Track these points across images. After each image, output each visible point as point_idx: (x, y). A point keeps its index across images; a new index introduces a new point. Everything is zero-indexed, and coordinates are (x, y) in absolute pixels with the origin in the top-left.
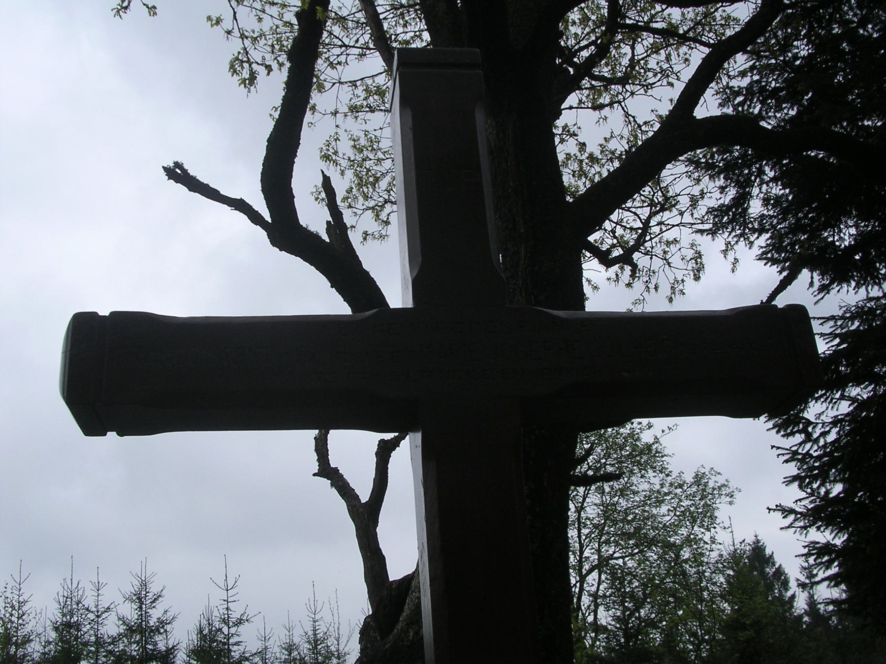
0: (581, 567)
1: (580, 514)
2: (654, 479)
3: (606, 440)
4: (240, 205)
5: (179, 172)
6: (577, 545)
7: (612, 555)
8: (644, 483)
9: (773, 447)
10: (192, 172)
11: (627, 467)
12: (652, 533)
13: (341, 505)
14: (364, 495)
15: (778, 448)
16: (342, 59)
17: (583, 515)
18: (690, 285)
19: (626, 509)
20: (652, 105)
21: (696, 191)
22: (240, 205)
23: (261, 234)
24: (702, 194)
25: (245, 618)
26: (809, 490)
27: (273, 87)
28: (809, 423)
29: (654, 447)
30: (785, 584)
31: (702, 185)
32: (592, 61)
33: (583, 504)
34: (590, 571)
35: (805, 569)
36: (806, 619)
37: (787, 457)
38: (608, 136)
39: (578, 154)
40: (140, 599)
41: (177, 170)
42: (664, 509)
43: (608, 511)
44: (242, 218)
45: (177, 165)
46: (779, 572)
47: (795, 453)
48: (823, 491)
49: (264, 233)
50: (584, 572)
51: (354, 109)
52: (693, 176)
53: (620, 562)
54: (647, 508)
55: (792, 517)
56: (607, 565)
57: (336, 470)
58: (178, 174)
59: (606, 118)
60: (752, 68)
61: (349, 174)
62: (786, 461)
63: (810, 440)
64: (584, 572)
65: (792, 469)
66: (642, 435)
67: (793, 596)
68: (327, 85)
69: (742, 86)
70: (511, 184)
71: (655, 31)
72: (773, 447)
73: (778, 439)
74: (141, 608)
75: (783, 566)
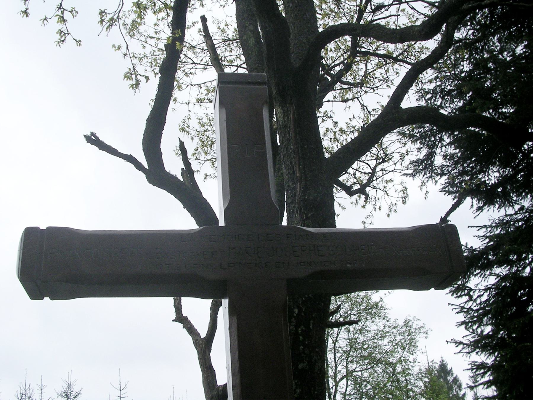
3: (351, 300)
4: (130, 159)
5: (94, 138)
6: (333, 363)
8: (374, 326)
9: (449, 304)
12: (379, 356)
13: (189, 339)
15: (452, 305)
17: (337, 345)
19: (363, 342)
20: (377, 100)
21: (403, 150)
22: (130, 159)
23: (142, 176)
26: (471, 330)
28: (471, 289)
29: (380, 304)
30: (460, 387)
32: (341, 74)
34: (342, 379)
39: (333, 128)
40: (67, 395)
41: (92, 137)
42: (386, 341)
43: (352, 343)
44: (131, 166)
45: (93, 134)
46: (456, 380)
47: (463, 308)
48: (479, 330)
50: (338, 380)
54: (376, 341)
55: (461, 346)
57: (186, 318)
58: (93, 140)
60: (436, 78)
61: (197, 139)
62: (458, 313)
63: (471, 300)
64: (338, 380)
65: (461, 317)
66: (372, 297)
67: (464, 395)
68: (184, 86)
70: (292, 147)
71: (379, 56)
72: (449, 304)
75: (458, 376)
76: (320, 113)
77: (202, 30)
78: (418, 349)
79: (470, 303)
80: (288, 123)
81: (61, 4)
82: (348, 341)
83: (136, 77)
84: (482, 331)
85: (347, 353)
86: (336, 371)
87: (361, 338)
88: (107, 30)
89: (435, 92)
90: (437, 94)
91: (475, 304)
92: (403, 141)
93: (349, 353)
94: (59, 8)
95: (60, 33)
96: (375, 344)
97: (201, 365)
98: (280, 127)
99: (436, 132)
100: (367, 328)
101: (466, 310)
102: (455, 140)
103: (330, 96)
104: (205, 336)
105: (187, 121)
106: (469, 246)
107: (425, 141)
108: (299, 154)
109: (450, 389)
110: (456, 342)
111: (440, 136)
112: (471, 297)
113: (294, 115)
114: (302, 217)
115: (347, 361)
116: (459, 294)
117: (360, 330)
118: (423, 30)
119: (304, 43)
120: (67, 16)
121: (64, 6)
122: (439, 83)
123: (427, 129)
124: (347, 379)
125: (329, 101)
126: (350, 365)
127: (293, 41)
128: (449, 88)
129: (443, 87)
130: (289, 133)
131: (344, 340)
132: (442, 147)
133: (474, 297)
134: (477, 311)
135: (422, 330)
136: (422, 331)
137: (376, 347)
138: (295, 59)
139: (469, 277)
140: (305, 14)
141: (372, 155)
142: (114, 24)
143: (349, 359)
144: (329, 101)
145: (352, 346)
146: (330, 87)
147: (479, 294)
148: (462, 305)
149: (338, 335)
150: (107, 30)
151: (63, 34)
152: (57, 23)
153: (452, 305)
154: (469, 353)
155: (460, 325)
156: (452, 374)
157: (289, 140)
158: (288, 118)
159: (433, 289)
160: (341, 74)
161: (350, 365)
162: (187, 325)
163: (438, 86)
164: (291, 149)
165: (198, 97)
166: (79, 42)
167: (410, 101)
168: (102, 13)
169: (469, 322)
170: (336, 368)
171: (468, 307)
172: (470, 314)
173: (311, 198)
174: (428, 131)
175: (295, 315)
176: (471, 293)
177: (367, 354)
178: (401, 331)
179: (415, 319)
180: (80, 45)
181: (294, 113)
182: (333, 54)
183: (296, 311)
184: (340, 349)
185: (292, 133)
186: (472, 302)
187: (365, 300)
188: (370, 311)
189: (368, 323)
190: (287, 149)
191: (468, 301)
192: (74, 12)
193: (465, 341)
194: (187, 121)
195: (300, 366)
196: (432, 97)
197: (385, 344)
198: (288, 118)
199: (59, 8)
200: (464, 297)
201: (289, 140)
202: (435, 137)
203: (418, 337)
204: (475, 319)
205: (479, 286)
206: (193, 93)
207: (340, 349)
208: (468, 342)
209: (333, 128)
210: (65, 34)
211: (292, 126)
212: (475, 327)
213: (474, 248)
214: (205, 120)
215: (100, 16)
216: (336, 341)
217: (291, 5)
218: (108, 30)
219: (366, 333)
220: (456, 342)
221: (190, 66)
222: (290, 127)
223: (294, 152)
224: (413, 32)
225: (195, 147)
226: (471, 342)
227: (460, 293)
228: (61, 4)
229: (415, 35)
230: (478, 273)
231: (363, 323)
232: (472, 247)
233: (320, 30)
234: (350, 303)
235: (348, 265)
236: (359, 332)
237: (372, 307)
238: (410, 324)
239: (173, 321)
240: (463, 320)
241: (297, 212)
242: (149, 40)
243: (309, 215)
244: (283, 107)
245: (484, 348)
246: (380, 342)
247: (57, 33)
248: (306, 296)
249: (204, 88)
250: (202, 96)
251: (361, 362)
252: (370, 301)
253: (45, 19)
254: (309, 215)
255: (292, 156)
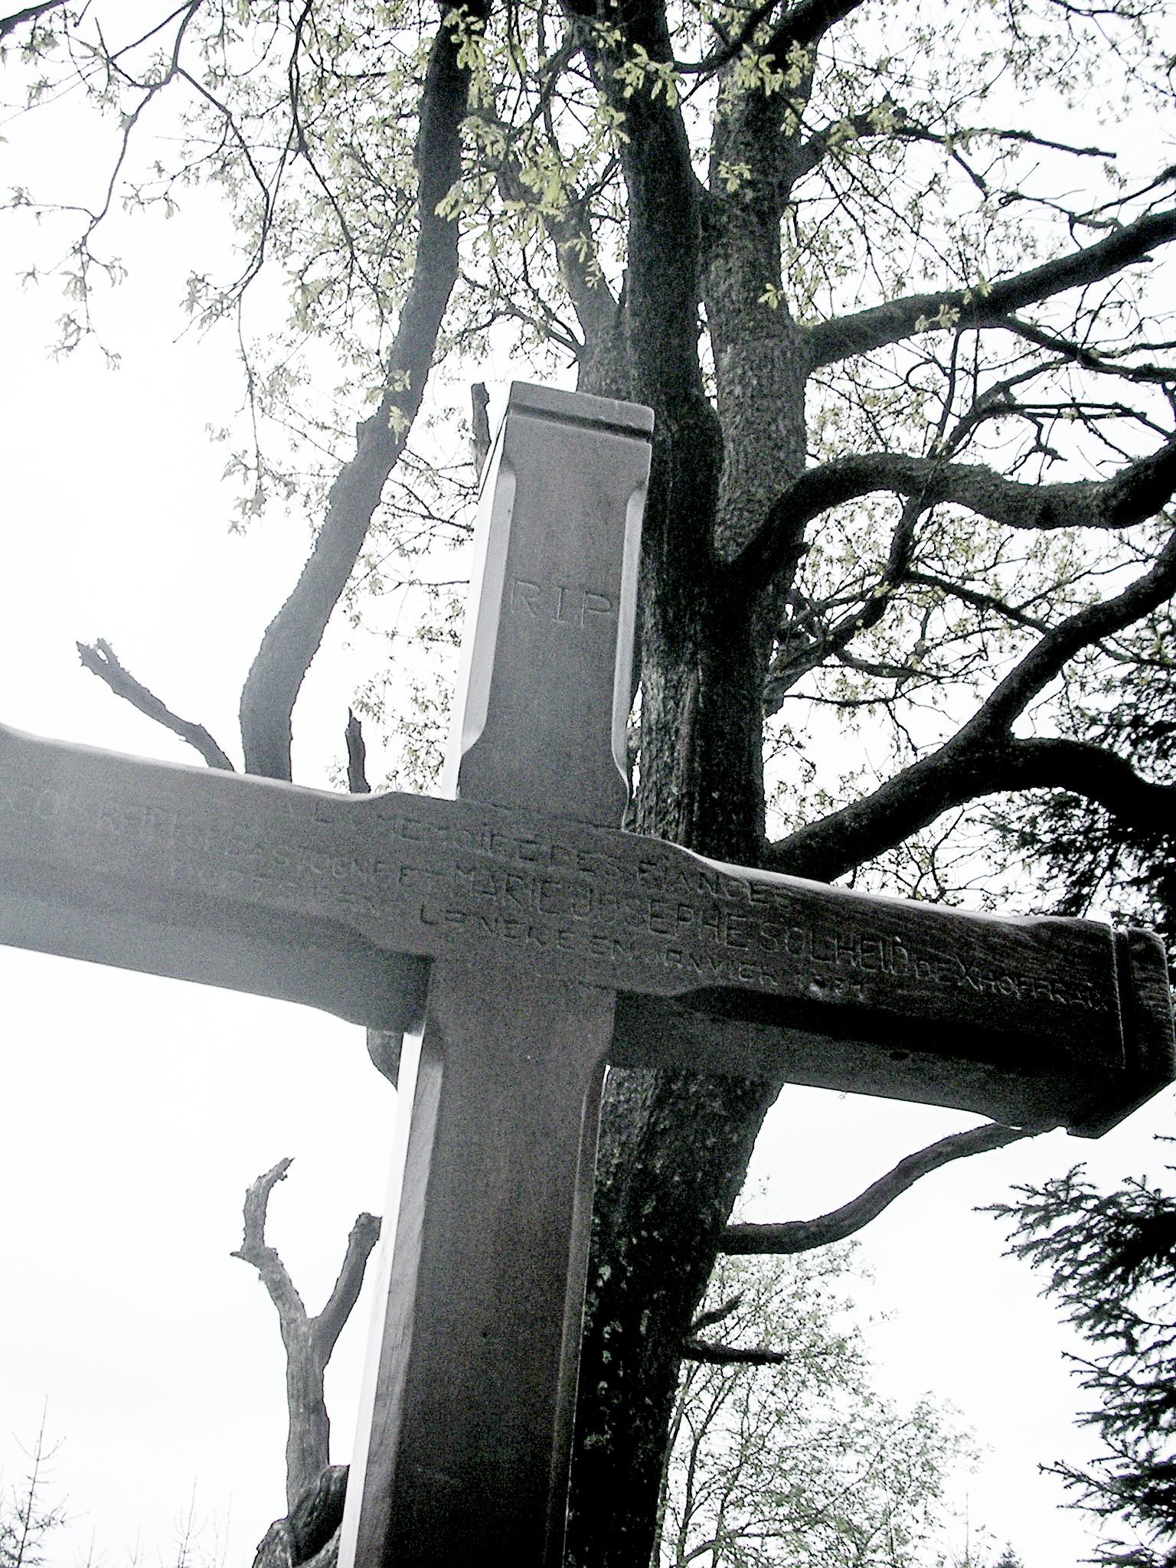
0: (682, 1542)
1: (697, 1442)
2: (842, 1399)
3: (767, 1319)
5: (103, 656)
6: (683, 1500)
7: (743, 1529)
8: (824, 1407)
9: (1065, 1354)
10: (125, 663)
11: (796, 1373)
12: (820, 1502)
13: (270, 1314)
14: (316, 1301)
15: (1074, 1358)
16: (421, 543)
17: (702, 1446)
18: (971, 103)
19: (782, 1450)
20: (939, 718)
21: (995, 886)
24: (1006, 894)
25: (58, 1517)
26: (1119, 1446)
27: (289, 540)
28: (1136, 1321)
29: (850, 1345)
31: (1007, 878)
32: (847, 631)
33: (705, 1427)
34: (700, 1551)
37: (1089, 1377)
38: (857, 770)
39: (800, 786)
41: (100, 653)
42: (850, 1459)
43: (749, 1447)
45: (102, 644)
47: (1104, 1372)
48: (1143, 1449)
50: (688, 1550)
51: (428, 635)
52: (994, 857)
53: (756, 1542)
54: (820, 1454)
55: (1081, 1488)
56: (731, 1544)
57: (273, 1254)
59: (856, 729)
60: (1127, 681)
61: (399, 741)
62: (1086, 1385)
63: (1133, 1353)
64: (688, 1550)
65: (1096, 1400)
66: (830, 1320)
68: (388, 584)
69: (1102, 709)
70: (675, 790)
71: (967, 596)
72: (1065, 1354)
73: (1076, 1340)
76: (773, 724)
77: (469, 425)
78: (944, 1499)
79: (1130, 1360)
80: (675, 719)
81: (84, 238)
82: (739, 1438)
83: (259, 478)
84: (1151, 1454)
85: (732, 1475)
86: (686, 1525)
87: (779, 1438)
88: (201, 327)
89: (1115, 724)
90: (1120, 727)
91: (1141, 1365)
92: (999, 858)
93: (736, 1478)
94: (78, 250)
95: (66, 325)
96: (816, 1464)
97: (290, 1396)
98: (650, 729)
99: (1100, 839)
100: (802, 1413)
101: (1110, 1381)
102: (1154, 872)
103: (809, 682)
104: (318, 1313)
105: (379, 687)
106: (1150, 1188)
107: (1066, 859)
108: (691, 812)
110: (1068, 1474)
111: (1110, 851)
112: (1132, 1343)
113: (695, 700)
115: (724, 1501)
116: (1097, 1330)
117: (780, 1414)
118: (1115, 496)
119: (760, 501)
120: (95, 276)
121: (91, 247)
122: (1131, 698)
123: (1076, 824)
124: (715, 1553)
125: (801, 696)
126: (732, 1512)
127: (726, 489)
128: (1158, 716)
129: (1141, 712)
130: (673, 747)
131: (728, 1435)
132: (1112, 885)
133: (1142, 1347)
134: (1148, 1388)
135: (964, 1445)
136: (963, 1449)
137: (819, 1473)
138: (729, 535)
139: (1136, 1282)
140: (775, 420)
141: (901, 884)
142: (226, 313)
143: (732, 1497)
144: (801, 696)
145: (747, 1458)
146: (813, 657)
147: (1159, 1338)
148: (1103, 1364)
149: (710, 1417)
150: (201, 327)
151: (73, 327)
152: (64, 293)
153: (1074, 1358)
154: (1102, 1512)
155: (1087, 1422)
157: (669, 769)
158: (677, 705)
159: (1061, 1131)
160: (847, 631)
161: (732, 1512)
162: (273, 1272)
163: (1130, 706)
164: (670, 794)
165: (424, 622)
166: (114, 357)
167: (1037, 722)
168: (197, 281)
169: (1118, 1417)
170: (689, 1512)
171: (1119, 1373)
172: (1122, 1394)
174: (1077, 832)
175: (600, 1283)
176: (1136, 1332)
177: (786, 1490)
178: (902, 1435)
179: (949, 1407)
180: (116, 367)
181: (698, 691)
182: (841, 547)
184: (709, 1461)
185: (682, 749)
186: (1135, 1358)
187: (810, 1325)
188: (819, 1360)
189: (807, 1397)
190: (658, 795)
191: (1122, 1354)
192: (117, 270)
193: (1098, 1474)
194: (379, 687)
196: (1106, 735)
197: (848, 1468)
198: (677, 705)
199: (78, 250)
200: (1112, 1339)
201: (669, 769)
202: (1095, 851)
203: (950, 1463)
204: (1137, 1411)
205: (1161, 1313)
206: (414, 609)
207: (709, 1461)
208: (1104, 1479)
209: (800, 786)
210: (79, 328)
211: (685, 730)
212: (1131, 1435)
213: (1163, 1195)
214: (432, 694)
215: (188, 289)
216: (703, 1433)
217: (738, 390)
218: (206, 326)
219: (797, 1426)
220: (1068, 1474)
221: (418, 525)
222: (677, 731)
224: (1085, 498)
225: (390, 771)
226: (1112, 1478)
227: (1101, 1326)
228: (84, 238)
229: (1088, 507)
230: (1167, 1276)
231: (791, 1395)
232: (1158, 1191)
233: (811, 464)
234: (762, 1326)
235: (814, 988)
236: (774, 1418)
237: (825, 1353)
238: (932, 1419)
239: (232, 1254)
240: (1099, 1410)
242: (312, 431)
244: (665, 674)
245: (1149, 1504)
246: (833, 1461)
247: (59, 322)
248: (644, 1233)
249: (444, 600)
250: (437, 623)
251: (766, 1509)
252: (822, 1331)
253: (32, 274)
255: (670, 818)
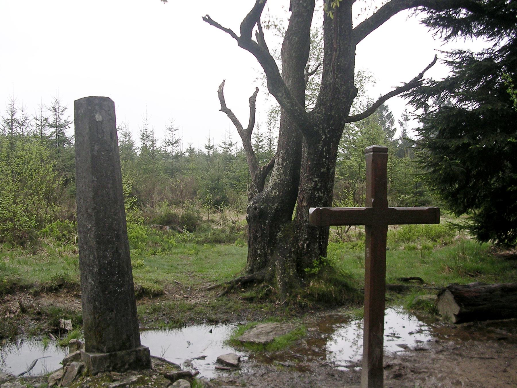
4: (229, 31)
22: (229, 31)
23: (235, 42)
30: (392, 122)
35: (404, 115)
36: (400, 141)
40: (55, 109)
44: (229, 35)
46: (390, 116)
49: (236, 42)
58: (208, 20)
67: (395, 129)
74: (56, 114)
75: (392, 112)
109: (384, 123)
114: (334, 76)
135: (371, 79)
156: (387, 110)
173: (342, 65)
183: (324, 137)
195: (322, 171)
223: (334, 29)
241: (331, 71)
243: (339, 76)
254: (339, 76)
